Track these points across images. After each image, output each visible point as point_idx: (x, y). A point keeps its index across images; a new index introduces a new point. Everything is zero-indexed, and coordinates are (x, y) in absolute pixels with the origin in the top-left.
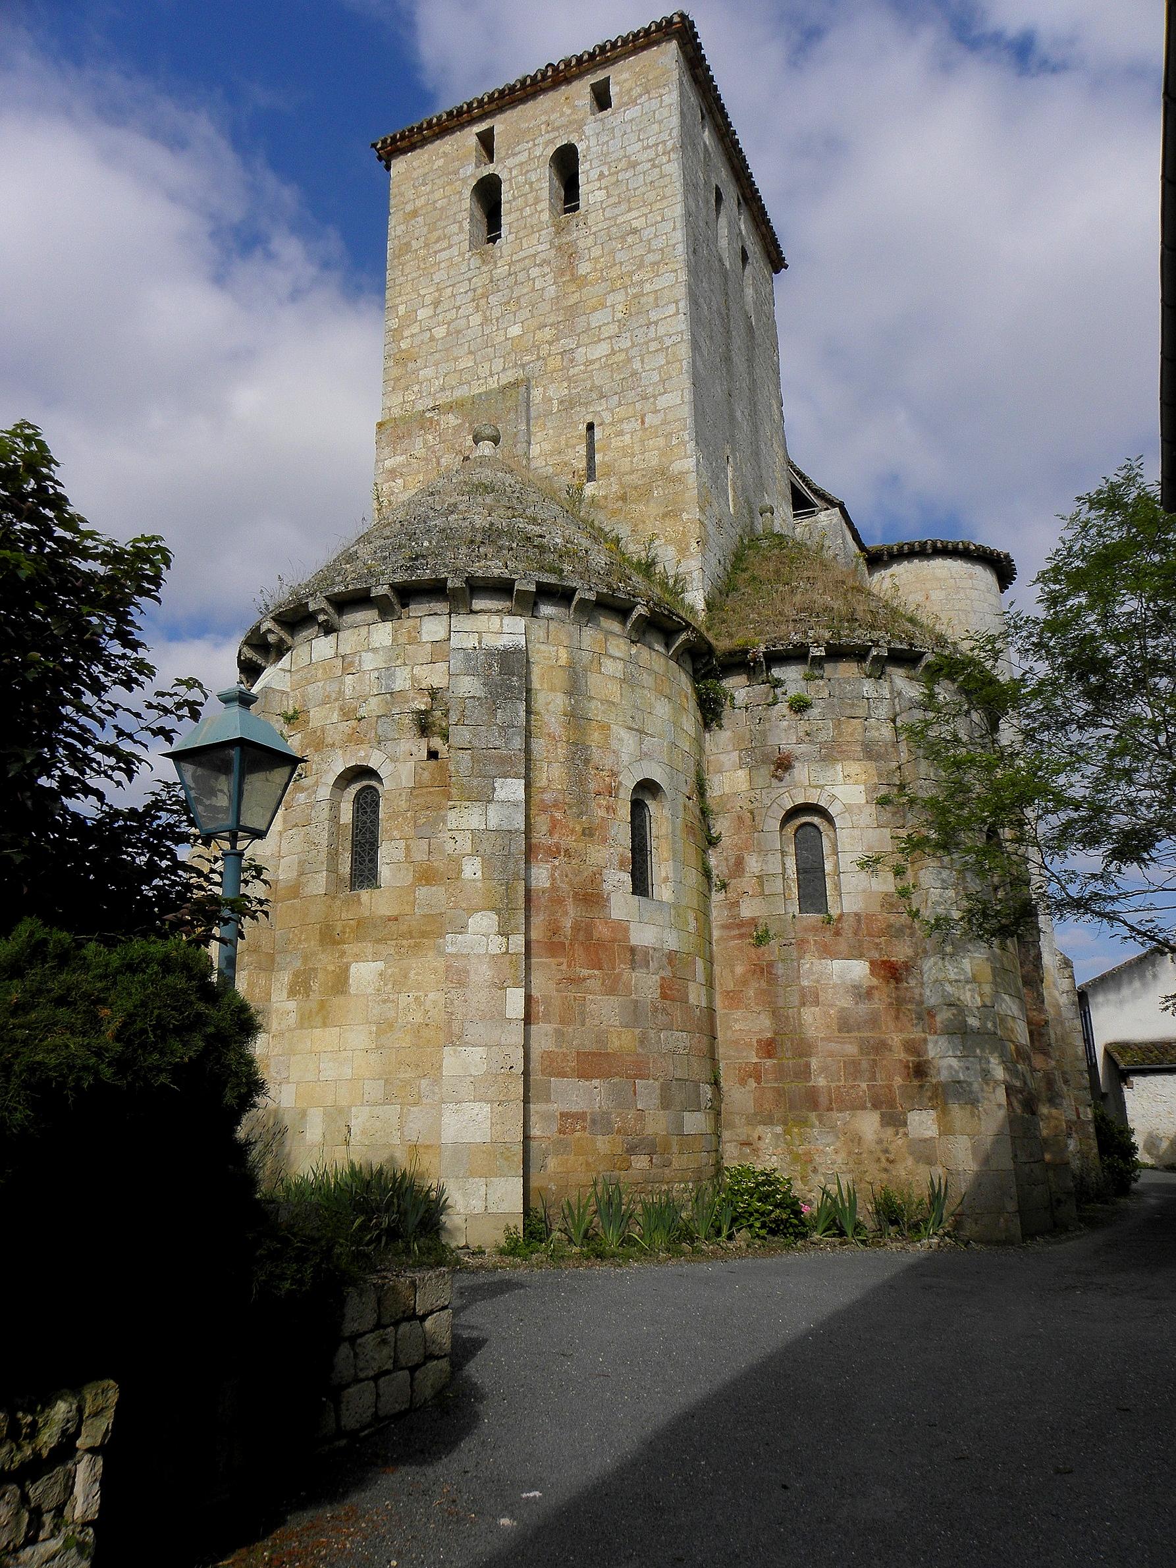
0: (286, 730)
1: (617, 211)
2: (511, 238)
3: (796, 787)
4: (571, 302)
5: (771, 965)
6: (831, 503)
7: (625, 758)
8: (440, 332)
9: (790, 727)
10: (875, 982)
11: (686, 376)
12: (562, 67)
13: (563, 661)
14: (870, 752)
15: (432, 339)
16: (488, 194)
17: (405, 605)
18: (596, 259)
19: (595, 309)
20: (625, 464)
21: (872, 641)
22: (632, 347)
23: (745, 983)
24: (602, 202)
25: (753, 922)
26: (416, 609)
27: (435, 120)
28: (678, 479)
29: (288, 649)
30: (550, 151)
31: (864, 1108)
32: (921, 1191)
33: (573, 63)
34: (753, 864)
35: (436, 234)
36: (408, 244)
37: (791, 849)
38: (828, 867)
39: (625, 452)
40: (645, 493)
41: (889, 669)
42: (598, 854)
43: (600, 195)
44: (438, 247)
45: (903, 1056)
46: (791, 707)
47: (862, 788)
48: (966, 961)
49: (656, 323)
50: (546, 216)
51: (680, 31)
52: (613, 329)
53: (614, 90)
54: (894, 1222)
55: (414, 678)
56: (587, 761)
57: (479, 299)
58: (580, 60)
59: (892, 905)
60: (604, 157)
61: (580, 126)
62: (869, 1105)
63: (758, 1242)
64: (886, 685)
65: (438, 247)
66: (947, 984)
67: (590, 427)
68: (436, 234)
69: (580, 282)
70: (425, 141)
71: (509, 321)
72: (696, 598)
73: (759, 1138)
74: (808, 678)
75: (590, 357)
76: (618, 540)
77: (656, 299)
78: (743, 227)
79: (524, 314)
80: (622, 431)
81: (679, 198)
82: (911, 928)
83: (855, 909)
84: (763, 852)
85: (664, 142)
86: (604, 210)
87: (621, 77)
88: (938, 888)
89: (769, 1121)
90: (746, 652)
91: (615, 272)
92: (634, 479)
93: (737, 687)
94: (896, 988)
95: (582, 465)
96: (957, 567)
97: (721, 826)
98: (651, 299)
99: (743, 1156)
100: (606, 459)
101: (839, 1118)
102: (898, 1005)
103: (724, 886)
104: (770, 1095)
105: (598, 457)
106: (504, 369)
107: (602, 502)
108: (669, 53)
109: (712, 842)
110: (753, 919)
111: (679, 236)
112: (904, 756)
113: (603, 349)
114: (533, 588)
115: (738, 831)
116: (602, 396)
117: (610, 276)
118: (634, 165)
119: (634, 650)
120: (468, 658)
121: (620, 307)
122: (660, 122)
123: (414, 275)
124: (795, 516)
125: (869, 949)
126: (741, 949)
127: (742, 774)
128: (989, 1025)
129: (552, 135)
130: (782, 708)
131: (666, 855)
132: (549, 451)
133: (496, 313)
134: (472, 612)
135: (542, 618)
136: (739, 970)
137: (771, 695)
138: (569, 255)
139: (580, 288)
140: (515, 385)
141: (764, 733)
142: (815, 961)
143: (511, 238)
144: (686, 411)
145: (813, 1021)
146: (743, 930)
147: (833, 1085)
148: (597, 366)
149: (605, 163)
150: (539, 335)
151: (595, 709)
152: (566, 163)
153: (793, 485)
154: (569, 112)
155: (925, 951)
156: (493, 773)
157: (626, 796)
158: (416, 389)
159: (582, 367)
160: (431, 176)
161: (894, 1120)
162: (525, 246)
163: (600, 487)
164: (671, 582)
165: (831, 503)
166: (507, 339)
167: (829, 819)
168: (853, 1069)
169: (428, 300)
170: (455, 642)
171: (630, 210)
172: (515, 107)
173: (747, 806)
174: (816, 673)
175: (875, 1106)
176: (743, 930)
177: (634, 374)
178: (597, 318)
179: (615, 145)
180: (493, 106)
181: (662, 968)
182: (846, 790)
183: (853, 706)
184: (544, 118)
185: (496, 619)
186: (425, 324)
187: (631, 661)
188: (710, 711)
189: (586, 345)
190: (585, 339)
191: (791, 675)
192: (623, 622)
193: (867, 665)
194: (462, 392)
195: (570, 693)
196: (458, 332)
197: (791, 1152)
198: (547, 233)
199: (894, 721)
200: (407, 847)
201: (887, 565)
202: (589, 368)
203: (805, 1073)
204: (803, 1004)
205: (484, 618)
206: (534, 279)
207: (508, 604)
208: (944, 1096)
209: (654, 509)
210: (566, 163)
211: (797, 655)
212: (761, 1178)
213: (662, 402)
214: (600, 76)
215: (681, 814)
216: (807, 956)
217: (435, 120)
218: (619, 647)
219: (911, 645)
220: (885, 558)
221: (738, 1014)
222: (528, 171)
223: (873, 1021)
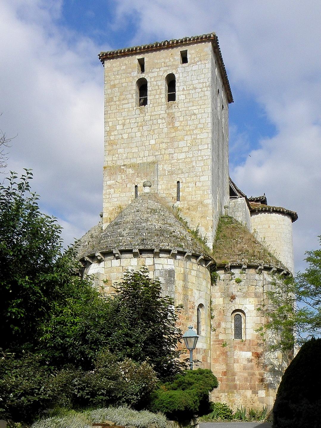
0: (104, 285)
1: (189, 105)
2: (151, 105)
3: (236, 304)
4: (172, 136)
5: (226, 352)
6: (243, 196)
8: (125, 136)
9: (235, 287)
10: (253, 358)
11: (210, 171)
12: (171, 43)
13: (182, 272)
14: (256, 296)
15: (122, 138)
16: (142, 86)
17: (141, 254)
18: (181, 122)
19: (180, 140)
20: (189, 198)
21: (259, 264)
22: (193, 157)
23: (219, 356)
24: (184, 100)
25: (222, 340)
26: (144, 255)
27: (123, 51)
28: (206, 206)
29: (103, 261)
30: (166, 75)
32: (261, 409)
33: (175, 42)
34: (223, 325)
35: (123, 97)
36: (112, 98)
37: (233, 321)
38: (243, 326)
39: (189, 194)
40: (196, 209)
41: (263, 271)
43: (183, 97)
44: (124, 102)
45: (258, 377)
46: (236, 281)
47: (253, 305)
48: (276, 353)
49: (201, 150)
51: (214, 41)
52: (186, 149)
53: (189, 56)
54: (254, 417)
56: (187, 300)
57: (140, 126)
58: (177, 42)
59: (259, 338)
61: (176, 68)
62: (249, 389)
63: (222, 420)
64: (262, 276)
66: (271, 359)
67: (178, 182)
68: (123, 97)
69: (176, 129)
70: (118, 57)
71: (150, 138)
72: (210, 244)
73: (221, 396)
74: (241, 273)
76: (187, 223)
77: (201, 141)
78: (223, 95)
79: (156, 136)
80: (189, 186)
81: (210, 105)
82: (263, 344)
83: (249, 339)
84: (226, 322)
85: (206, 82)
87: (192, 51)
88: (273, 337)
89: (224, 392)
90: (225, 265)
91: (187, 128)
92: (192, 203)
93: (221, 273)
94: (258, 359)
95: (175, 195)
96: (277, 215)
97: (214, 313)
98: (200, 141)
99: (216, 400)
101: (242, 391)
102: (258, 364)
103: (215, 330)
104: (225, 386)
106: (149, 156)
108: (208, 46)
109: (212, 318)
110: (222, 340)
111: (209, 120)
112: (265, 297)
113: (183, 156)
114: (176, 252)
115: (219, 315)
116: (182, 173)
117: (186, 129)
118: (195, 88)
119: (199, 267)
120: (160, 272)
121: (189, 142)
122: (205, 74)
123: (115, 111)
124: (230, 198)
125: (252, 349)
126: (218, 347)
127: (221, 299)
128: (280, 369)
129: (166, 68)
130: (233, 281)
131: (204, 323)
132: (164, 188)
133: (146, 133)
134: (159, 257)
135: (178, 259)
136: (218, 353)
137: (231, 277)
138: (172, 118)
139: (176, 131)
140: (154, 163)
141: (228, 288)
142: (238, 352)
143: (151, 105)
144: (210, 183)
145: (237, 367)
146: (219, 342)
147: (241, 383)
148: (181, 161)
149: (185, 85)
151: (190, 285)
152: (171, 81)
153: (230, 186)
154: (172, 60)
155: (266, 350)
157: (196, 308)
158: (117, 156)
159: (176, 161)
160: (120, 72)
161: (255, 392)
162: (156, 110)
163: (181, 204)
164: (203, 239)
165: (243, 196)
166: (150, 144)
167: (244, 314)
168: (246, 379)
169: (120, 122)
170: (157, 267)
171: (193, 106)
172: (152, 52)
173: (222, 308)
174: (244, 272)
175: (251, 389)
176: (219, 342)
177: (193, 167)
178: (182, 144)
180: (145, 50)
181: (203, 353)
182: (249, 306)
183: (252, 282)
184: (163, 60)
185: (166, 260)
186: (120, 132)
187: (198, 270)
188: (213, 280)
189: (177, 153)
190: (177, 151)
191: (236, 271)
192: (196, 260)
193: (257, 270)
194: (133, 161)
195: (184, 281)
196: (132, 138)
197: (229, 400)
198: (164, 107)
199: (263, 287)
201: (257, 214)
202: (178, 162)
205: (162, 259)
206: (159, 124)
207: (169, 255)
208: (268, 386)
209: (198, 215)
210: (171, 81)
211: (239, 267)
212: (223, 406)
213: (202, 179)
214: (184, 48)
215: (207, 312)
216: (236, 350)
217: (123, 51)
218: (195, 267)
219: (270, 265)
220: (257, 211)
221: (217, 364)
222: (157, 81)
223: (252, 368)
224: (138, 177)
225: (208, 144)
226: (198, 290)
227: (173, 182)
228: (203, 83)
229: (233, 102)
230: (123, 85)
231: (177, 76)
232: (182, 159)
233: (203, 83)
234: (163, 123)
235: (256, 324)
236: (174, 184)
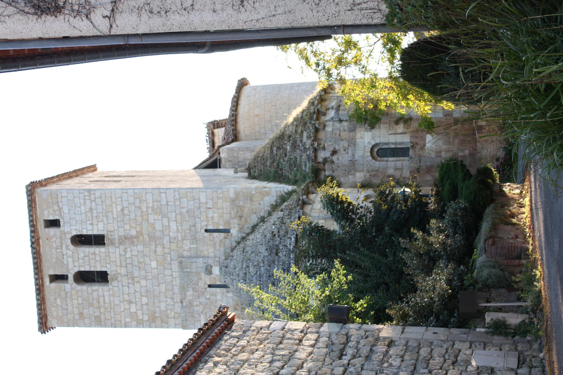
1: (111, 217)
20: (226, 216)
24: (104, 224)
67: (206, 231)
75: (175, 230)
91: (139, 219)
98: (156, 204)
113: (173, 225)
122: (74, 197)
162: (114, 260)
178: (158, 226)
196: (147, 291)
230: (80, 302)
231: (74, 233)
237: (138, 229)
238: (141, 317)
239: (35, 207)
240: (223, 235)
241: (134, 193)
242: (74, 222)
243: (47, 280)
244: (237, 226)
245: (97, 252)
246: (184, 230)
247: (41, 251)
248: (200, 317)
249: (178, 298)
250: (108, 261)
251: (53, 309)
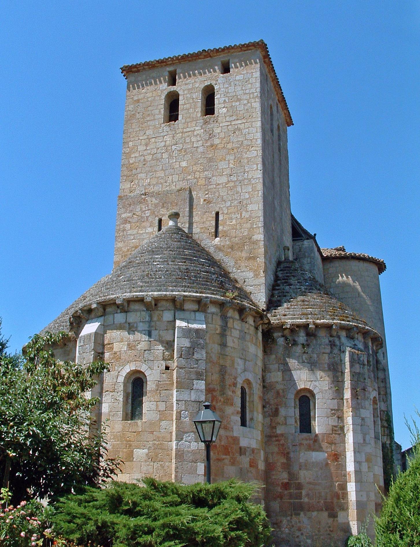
1: (231, 119)
7: (239, 371)
20: (233, 233)
24: (225, 113)
28: (256, 242)
30: (202, 86)
31: (322, 510)
42: (229, 410)
50: (199, 115)
51: (262, 46)
55: (159, 335)
60: (226, 94)
62: (324, 509)
65: (148, 119)
67: (217, 214)
75: (218, 182)
85: (253, 93)
86: (226, 117)
91: (229, 146)
98: (246, 161)
100: (225, 229)
105: (220, 228)
107: (222, 248)
113: (223, 180)
121: (232, 162)
122: (251, 84)
127: (280, 374)
144: (261, 214)
150: (195, 168)
156: (193, 378)
159: (214, 186)
162: (189, 126)
175: (326, 510)
178: (222, 165)
179: (231, 89)
181: (250, 455)
183: (325, 348)
196: (157, 159)
200: (157, 405)
203: (299, 496)
204: (300, 469)
224: (163, 207)
225: (257, 165)
226: (241, 359)
227: (211, 212)
228: (250, 94)
229: (293, 124)
230: (149, 99)
231: (216, 87)
232: (223, 183)
233: (250, 94)
234: (198, 141)
235: (332, 410)
236: (212, 215)
237: (220, 146)
238: (133, 156)
239: (241, 51)
240: (213, 230)
241: (256, 139)
242: (227, 86)
243: (171, 69)
244: (222, 244)
245: (245, 192)
246: (218, 191)
247: (199, 60)
248: (129, 213)
249: (151, 189)
250: (188, 120)
251: (144, 76)
